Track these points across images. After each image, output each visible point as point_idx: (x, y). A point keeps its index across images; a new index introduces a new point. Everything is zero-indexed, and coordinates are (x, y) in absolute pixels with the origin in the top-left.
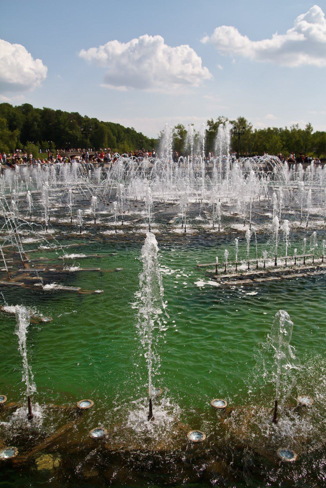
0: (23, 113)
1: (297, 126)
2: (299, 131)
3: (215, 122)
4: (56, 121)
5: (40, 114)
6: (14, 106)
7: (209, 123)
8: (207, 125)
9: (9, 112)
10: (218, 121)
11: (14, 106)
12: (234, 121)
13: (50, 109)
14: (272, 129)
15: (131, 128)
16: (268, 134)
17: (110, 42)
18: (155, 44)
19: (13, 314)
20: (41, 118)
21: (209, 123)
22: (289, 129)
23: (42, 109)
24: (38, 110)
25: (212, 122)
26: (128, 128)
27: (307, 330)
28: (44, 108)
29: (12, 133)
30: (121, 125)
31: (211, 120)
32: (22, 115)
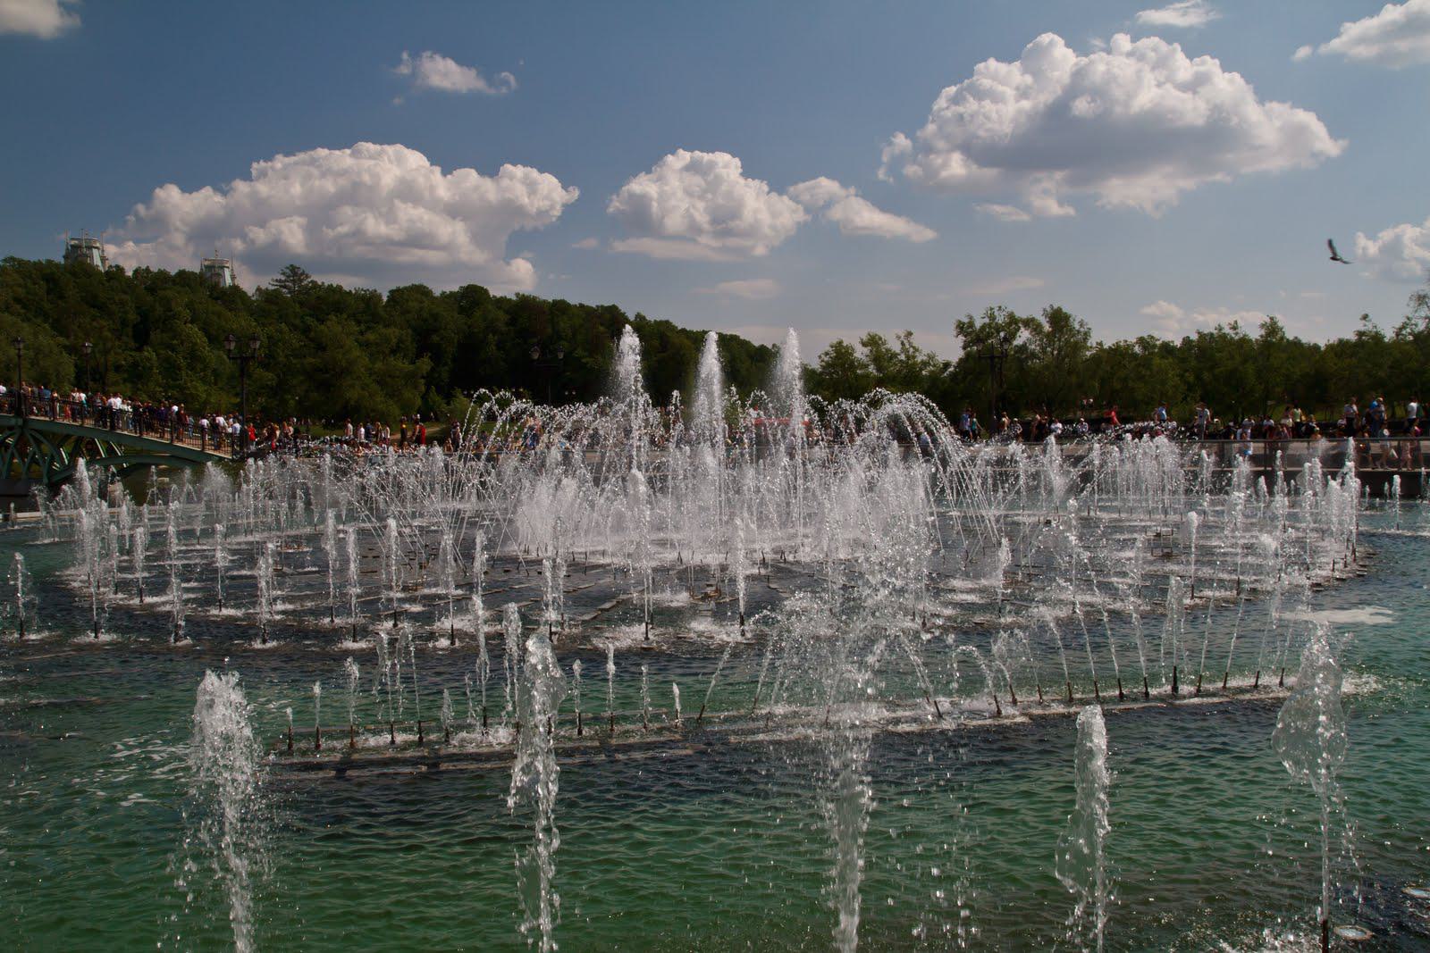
0: (462, 310)
1: (1234, 328)
2: (1244, 341)
3: (978, 324)
4: (549, 330)
5: (507, 312)
6: (437, 293)
7: (962, 328)
8: (955, 333)
9: (421, 309)
10: (987, 320)
11: (437, 293)
12: (1033, 320)
13: (534, 298)
14: (1194, 337)
15: (770, 347)
16: (1153, 354)
17: (399, 147)
18: (1051, 43)
19: (169, 612)
20: (507, 324)
21: (962, 328)
22: (1389, 335)
23: (514, 298)
24: (501, 302)
25: (971, 324)
26: (763, 347)
27: (426, 591)
28: (517, 295)
29: (411, 367)
30: (742, 338)
31: (966, 320)
32: (456, 315)
